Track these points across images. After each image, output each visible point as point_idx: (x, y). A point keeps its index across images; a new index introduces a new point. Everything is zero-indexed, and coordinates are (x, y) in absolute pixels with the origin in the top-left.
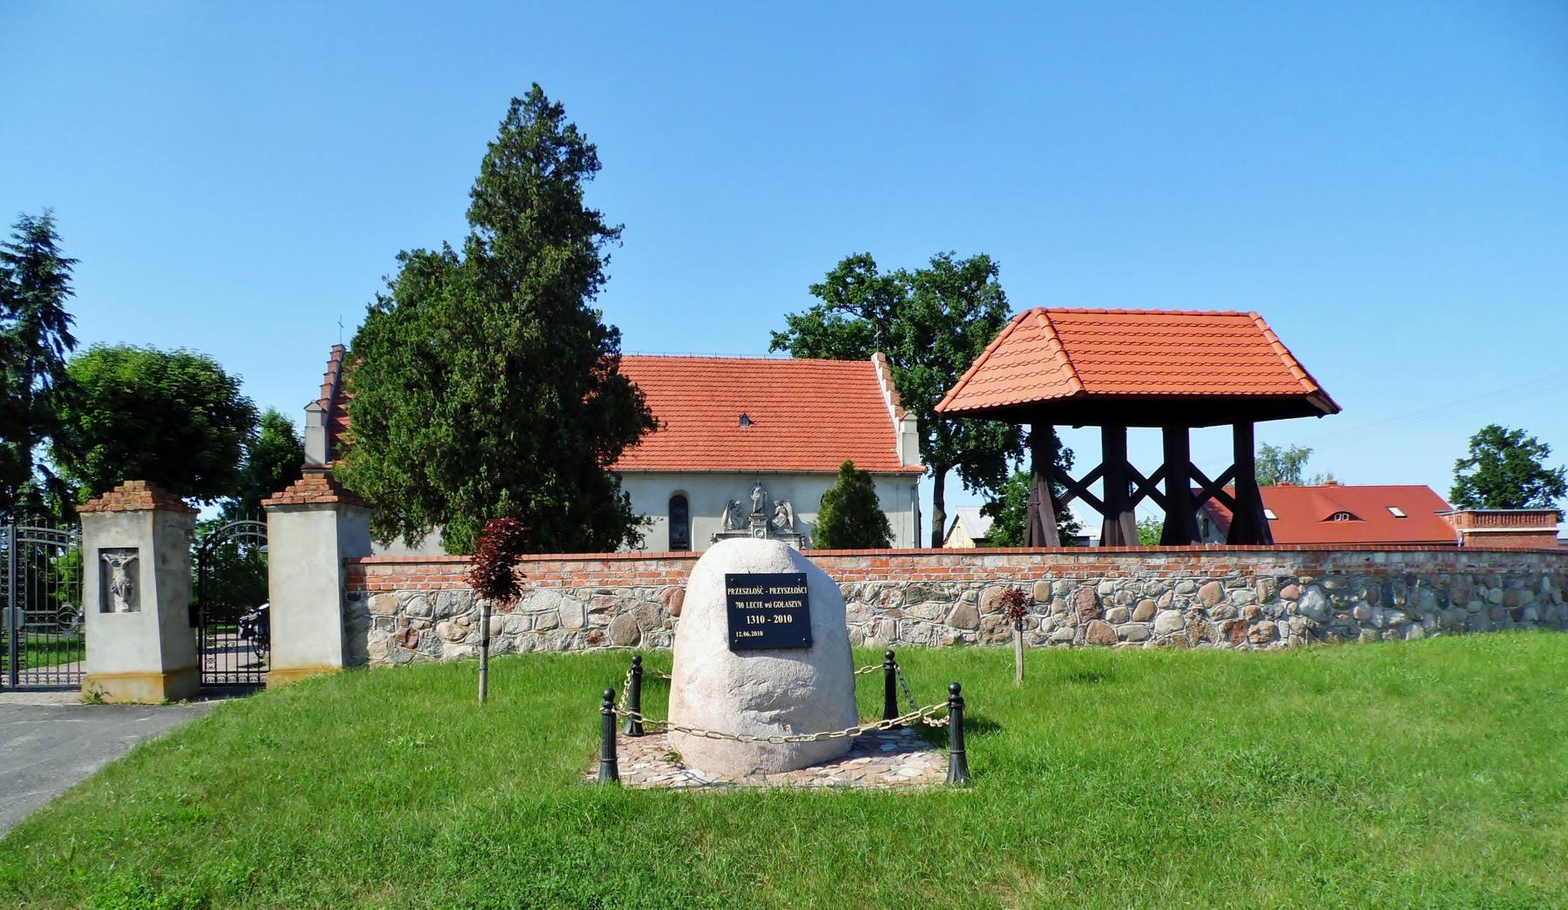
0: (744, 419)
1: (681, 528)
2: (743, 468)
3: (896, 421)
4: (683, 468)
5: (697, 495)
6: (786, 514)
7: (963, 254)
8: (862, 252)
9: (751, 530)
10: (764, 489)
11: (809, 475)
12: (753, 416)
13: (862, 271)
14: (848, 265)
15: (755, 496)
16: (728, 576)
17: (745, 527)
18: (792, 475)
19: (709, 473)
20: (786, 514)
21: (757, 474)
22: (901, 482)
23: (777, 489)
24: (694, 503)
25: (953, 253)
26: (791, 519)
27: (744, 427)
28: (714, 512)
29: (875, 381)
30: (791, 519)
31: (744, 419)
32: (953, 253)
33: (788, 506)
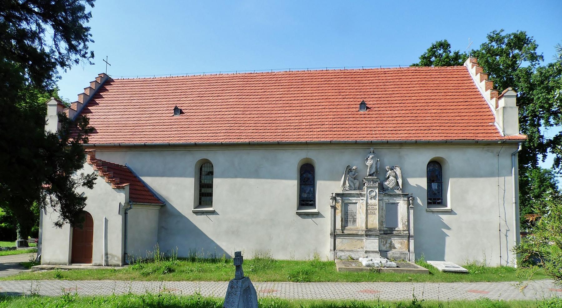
0: (363, 105)
1: (308, 189)
2: (359, 140)
3: (492, 103)
4: (309, 140)
5: (322, 162)
6: (396, 177)
7: (509, 29)
8: (441, 39)
9: (365, 191)
10: (376, 156)
11: (417, 144)
12: (369, 103)
13: (441, 52)
14: (433, 51)
15: (369, 163)
16: (240, 253)
17: (360, 188)
18: (401, 144)
19: (331, 144)
20: (396, 177)
21: (371, 144)
22: (503, 149)
23: (388, 157)
24: (319, 170)
25: (502, 31)
26: (400, 181)
27: (362, 112)
28: (334, 177)
29: (469, 78)
30: (400, 181)
31: (363, 105)
32: (502, 31)
33: (398, 171)
